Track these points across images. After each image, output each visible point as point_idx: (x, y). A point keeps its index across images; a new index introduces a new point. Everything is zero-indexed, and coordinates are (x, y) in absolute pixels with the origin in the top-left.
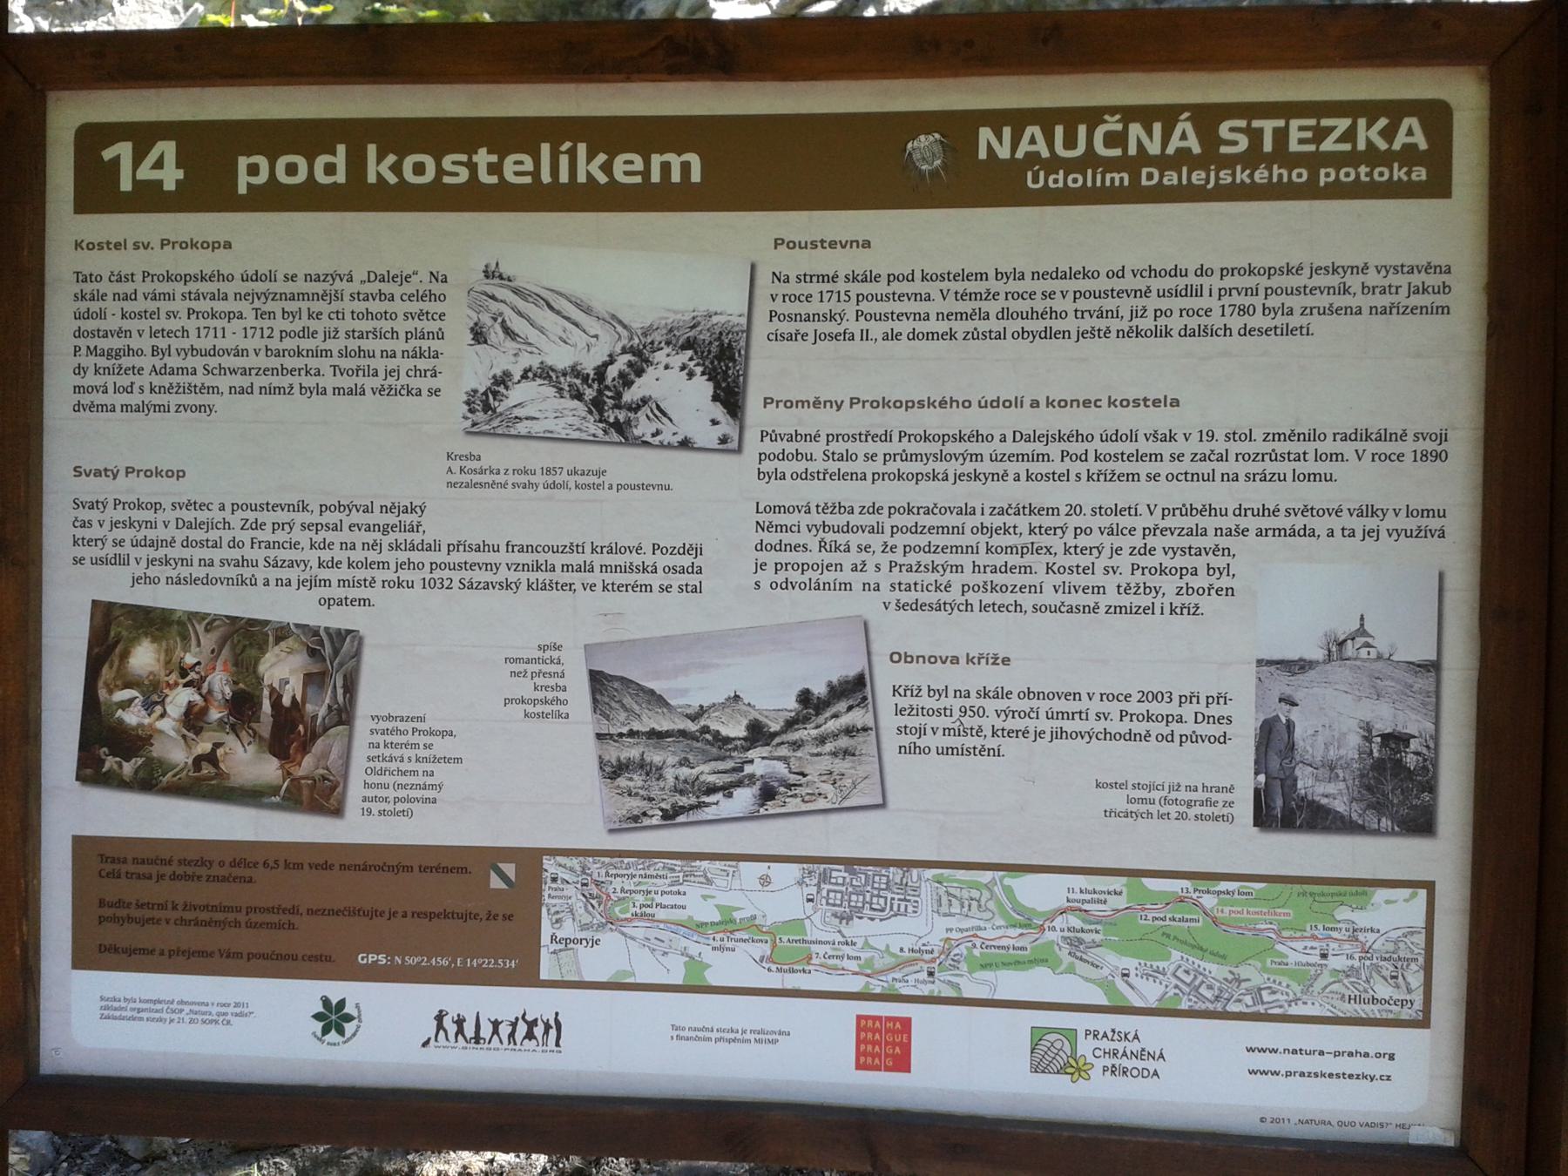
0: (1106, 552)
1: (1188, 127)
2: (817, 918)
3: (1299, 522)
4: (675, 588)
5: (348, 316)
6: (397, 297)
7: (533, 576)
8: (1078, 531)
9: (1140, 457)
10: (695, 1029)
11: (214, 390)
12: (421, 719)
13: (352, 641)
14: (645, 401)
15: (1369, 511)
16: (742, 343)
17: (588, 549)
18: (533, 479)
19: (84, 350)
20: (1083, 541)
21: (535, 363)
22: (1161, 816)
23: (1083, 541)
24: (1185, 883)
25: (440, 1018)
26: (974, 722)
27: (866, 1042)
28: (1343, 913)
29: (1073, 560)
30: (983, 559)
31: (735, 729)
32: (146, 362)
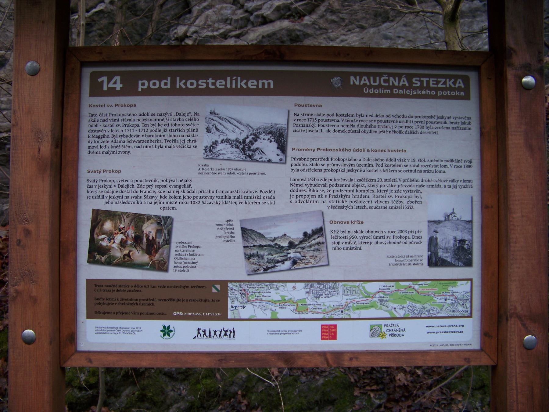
0: (389, 192)
1: (405, 79)
2: (309, 298)
3: (437, 183)
4: (267, 203)
5: (170, 125)
6: (185, 120)
7: (224, 200)
8: (381, 186)
9: (397, 166)
10: (275, 331)
11: (130, 147)
12: (191, 243)
13: (170, 220)
14: (257, 149)
15: (454, 181)
16: (286, 133)
17: (241, 192)
18: (224, 172)
19: (91, 136)
20: (382, 189)
21: (225, 138)
22: (404, 265)
23: (382, 189)
24: (411, 283)
25: (198, 330)
26: (354, 240)
27: (324, 332)
28: (450, 288)
29: (379, 194)
30: (355, 194)
31: (285, 244)
32: (110, 139)
